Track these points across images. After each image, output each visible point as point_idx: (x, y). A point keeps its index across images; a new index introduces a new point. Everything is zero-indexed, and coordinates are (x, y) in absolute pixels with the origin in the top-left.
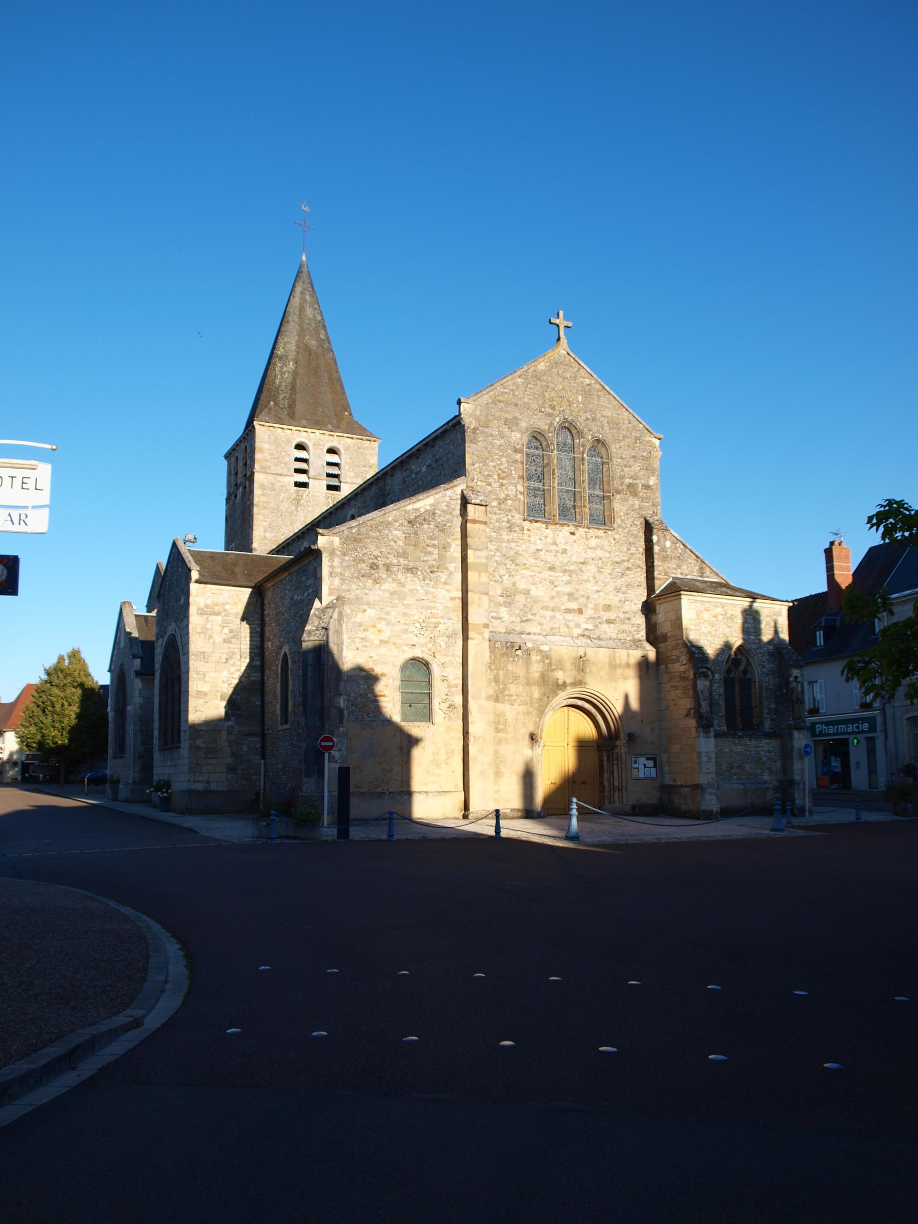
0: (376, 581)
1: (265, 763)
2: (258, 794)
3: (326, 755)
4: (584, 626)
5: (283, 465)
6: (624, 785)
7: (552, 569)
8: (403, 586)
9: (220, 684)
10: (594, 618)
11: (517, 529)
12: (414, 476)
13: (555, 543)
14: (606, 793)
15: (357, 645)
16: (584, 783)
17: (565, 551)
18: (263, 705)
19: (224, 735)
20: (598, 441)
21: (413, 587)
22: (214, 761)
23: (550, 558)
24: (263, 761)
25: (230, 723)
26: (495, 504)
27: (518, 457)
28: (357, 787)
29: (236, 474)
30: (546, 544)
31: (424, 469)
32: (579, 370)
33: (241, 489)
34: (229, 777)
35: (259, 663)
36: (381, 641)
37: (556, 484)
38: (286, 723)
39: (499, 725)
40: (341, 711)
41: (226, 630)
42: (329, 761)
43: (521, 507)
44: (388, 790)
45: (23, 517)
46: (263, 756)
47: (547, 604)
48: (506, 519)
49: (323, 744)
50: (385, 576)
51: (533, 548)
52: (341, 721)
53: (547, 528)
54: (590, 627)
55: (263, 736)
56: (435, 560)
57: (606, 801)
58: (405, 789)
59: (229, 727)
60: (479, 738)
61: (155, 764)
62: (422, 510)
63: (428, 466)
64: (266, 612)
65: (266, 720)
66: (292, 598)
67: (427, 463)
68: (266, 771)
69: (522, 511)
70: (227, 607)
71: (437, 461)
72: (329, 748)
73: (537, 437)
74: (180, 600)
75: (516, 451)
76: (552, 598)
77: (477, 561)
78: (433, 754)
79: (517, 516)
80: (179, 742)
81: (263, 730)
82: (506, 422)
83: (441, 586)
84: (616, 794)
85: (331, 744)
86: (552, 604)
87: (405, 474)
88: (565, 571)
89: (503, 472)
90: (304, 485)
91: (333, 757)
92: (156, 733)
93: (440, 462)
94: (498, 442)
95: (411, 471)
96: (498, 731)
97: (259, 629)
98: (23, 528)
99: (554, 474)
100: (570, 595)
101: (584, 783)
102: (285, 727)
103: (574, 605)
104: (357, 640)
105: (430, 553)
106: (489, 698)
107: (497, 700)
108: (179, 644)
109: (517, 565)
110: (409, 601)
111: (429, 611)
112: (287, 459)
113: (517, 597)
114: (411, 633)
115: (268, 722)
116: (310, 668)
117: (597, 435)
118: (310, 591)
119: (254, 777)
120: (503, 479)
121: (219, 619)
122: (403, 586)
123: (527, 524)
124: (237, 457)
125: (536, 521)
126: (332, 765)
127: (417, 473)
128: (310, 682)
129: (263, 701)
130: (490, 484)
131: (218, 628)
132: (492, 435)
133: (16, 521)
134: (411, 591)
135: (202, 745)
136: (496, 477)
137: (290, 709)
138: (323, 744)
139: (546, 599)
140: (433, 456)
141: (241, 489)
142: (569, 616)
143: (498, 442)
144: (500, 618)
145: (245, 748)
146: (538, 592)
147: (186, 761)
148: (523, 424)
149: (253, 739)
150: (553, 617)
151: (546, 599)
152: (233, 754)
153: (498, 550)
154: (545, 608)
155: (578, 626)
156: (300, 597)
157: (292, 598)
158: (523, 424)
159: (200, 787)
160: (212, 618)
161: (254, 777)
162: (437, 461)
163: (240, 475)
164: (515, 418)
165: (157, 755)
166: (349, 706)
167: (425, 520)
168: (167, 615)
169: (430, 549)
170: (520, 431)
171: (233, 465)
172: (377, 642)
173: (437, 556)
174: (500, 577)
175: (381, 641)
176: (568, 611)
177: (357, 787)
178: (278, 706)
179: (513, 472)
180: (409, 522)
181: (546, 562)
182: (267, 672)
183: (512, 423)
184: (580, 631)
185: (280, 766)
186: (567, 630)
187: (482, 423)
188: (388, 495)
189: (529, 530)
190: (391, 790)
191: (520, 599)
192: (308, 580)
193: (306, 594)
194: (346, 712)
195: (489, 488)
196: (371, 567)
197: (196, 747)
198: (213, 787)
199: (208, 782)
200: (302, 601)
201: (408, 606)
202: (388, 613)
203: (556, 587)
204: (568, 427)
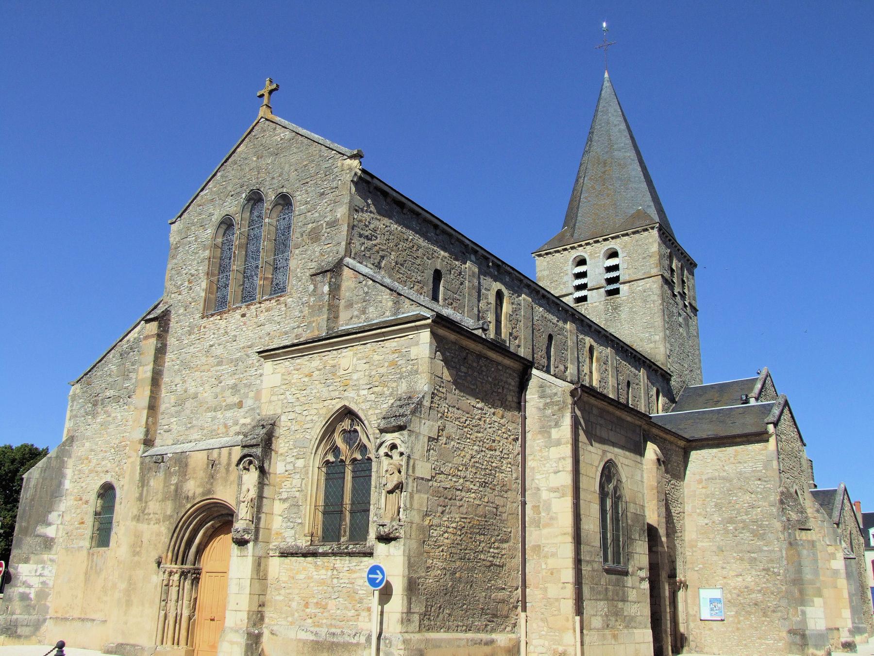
4: (242, 421)
62: (132, 339)
142: (229, 414)
146: (207, 394)
150: (213, 419)
154: (209, 409)
155: (236, 423)
172: (87, 471)
186: (224, 430)
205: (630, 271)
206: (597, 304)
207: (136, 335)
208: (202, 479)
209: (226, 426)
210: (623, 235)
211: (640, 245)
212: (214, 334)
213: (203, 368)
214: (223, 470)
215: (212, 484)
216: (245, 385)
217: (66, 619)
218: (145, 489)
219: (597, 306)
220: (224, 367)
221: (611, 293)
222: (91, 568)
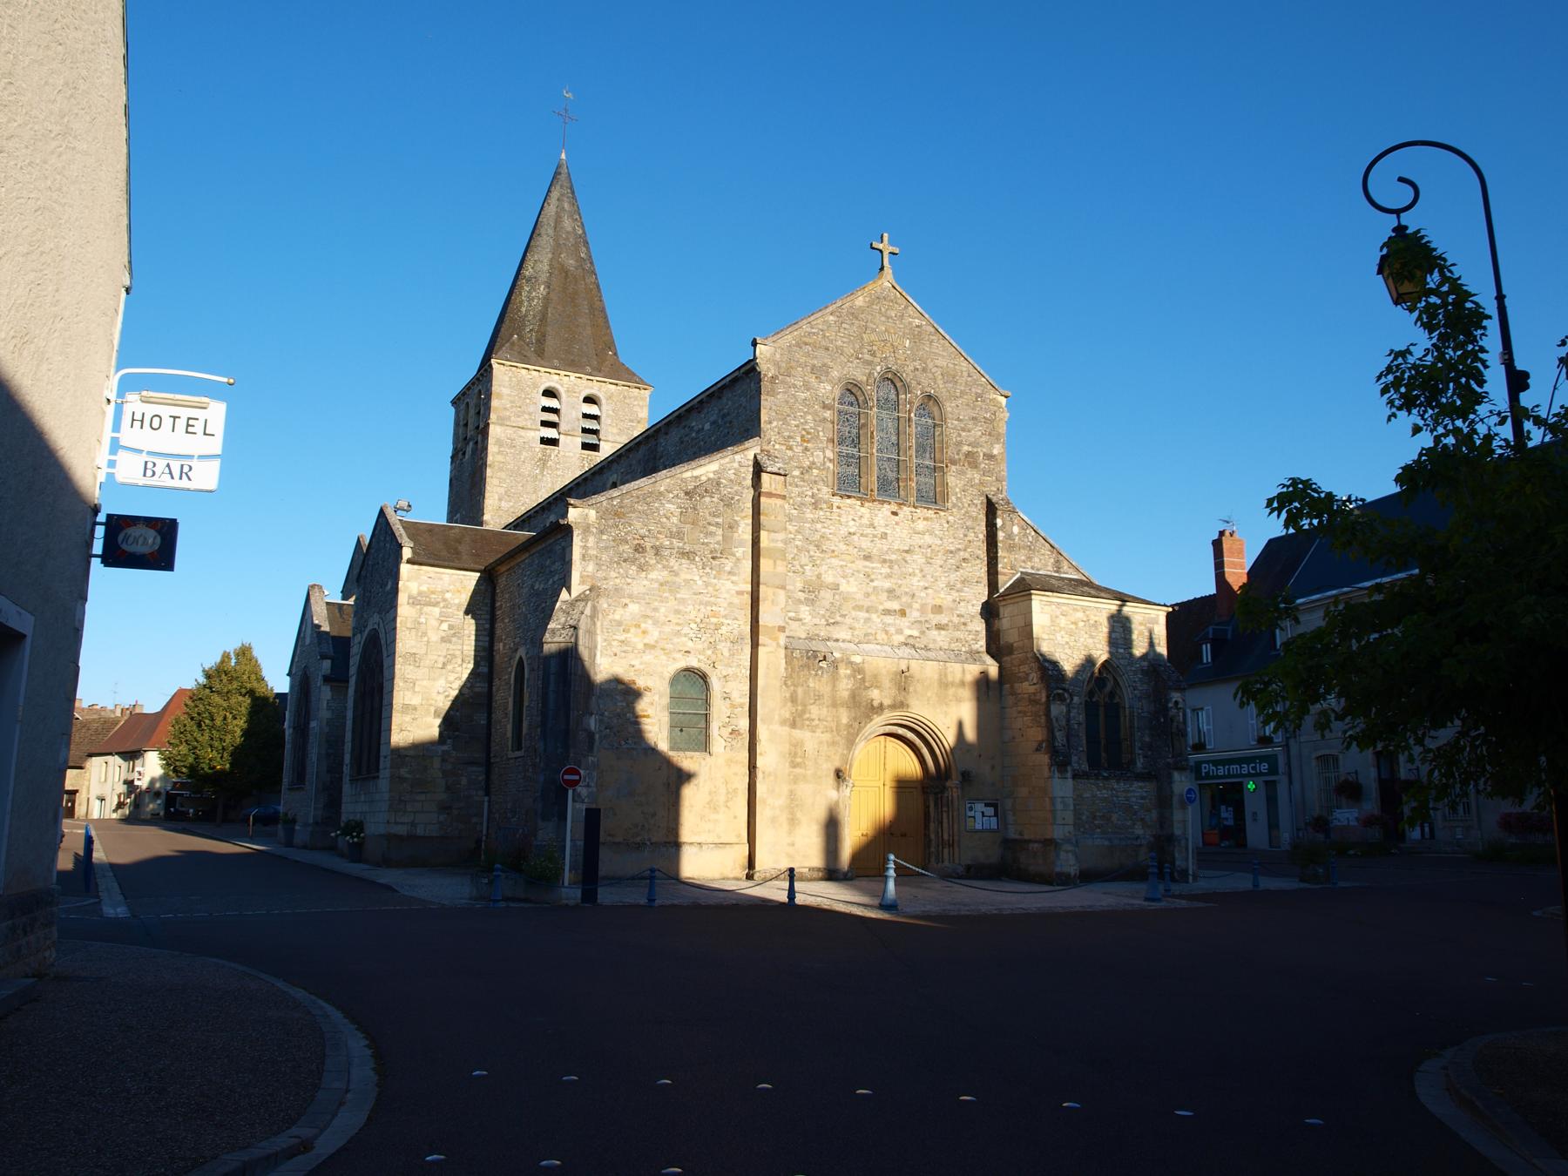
0: (641, 568)
2: (479, 841)
3: (570, 792)
4: (908, 632)
7: (867, 558)
8: (677, 574)
9: (434, 695)
13: (872, 526)
16: (903, 835)
17: (884, 536)
19: (437, 763)
25: (445, 748)
26: (796, 473)
27: (828, 414)
30: (861, 525)
31: (707, 426)
34: (442, 818)
35: (485, 670)
38: (519, 748)
39: (795, 757)
40: (591, 735)
41: (445, 626)
45: (186, 469)
46: (488, 793)
51: (844, 531)
55: (488, 766)
61: (344, 799)
63: (713, 423)
68: (490, 811)
71: (724, 416)
72: (575, 783)
73: (852, 390)
76: (867, 595)
79: (825, 489)
80: (378, 770)
86: (867, 603)
88: (885, 561)
90: (553, 442)
92: (347, 758)
95: (691, 428)
96: (794, 765)
98: (184, 483)
100: (890, 591)
101: (903, 835)
102: (518, 754)
106: (783, 722)
112: (531, 409)
115: (494, 748)
119: (474, 820)
121: (436, 610)
122: (677, 574)
123: (836, 500)
126: (578, 805)
130: (790, 448)
132: (795, 386)
133: (176, 473)
134: (687, 581)
137: (525, 731)
139: (859, 596)
142: (889, 619)
145: (464, 781)
146: (850, 587)
148: (835, 374)
151: (859, 596)
152: (448, 788)
154: (858, 608)
158: (835, 374)
159: (402, 830)
160: (427, 609)
161: (474, 820)
162: (724, 416)
163: (470, 426)
165: (347, 788)
170: (830, 382)
172: (640, 646)
176: (887, 612)
178: (510, 727)
180: (687, 493)
181: (860, 549)
182: (496, 682)
183: (820, 372)
191: (826, 595)
195: (790, 453)
198: (420, 831)
199: (413, 824)
201: (683, 601)
204: (892, 379)
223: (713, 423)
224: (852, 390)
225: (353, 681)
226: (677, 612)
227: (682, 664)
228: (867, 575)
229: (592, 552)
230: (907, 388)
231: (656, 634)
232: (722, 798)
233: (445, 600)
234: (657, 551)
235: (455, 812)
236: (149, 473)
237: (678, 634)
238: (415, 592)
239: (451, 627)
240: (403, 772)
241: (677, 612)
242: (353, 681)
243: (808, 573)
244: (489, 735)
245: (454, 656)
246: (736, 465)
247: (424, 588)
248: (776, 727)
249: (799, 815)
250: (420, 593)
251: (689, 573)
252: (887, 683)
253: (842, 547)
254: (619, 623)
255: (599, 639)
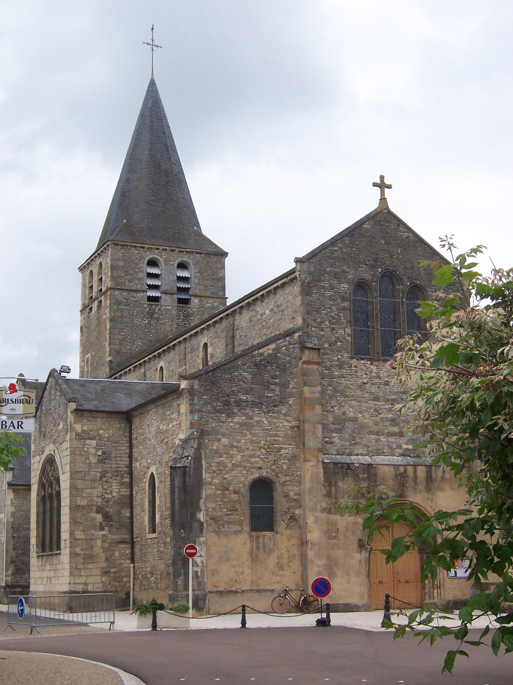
0: (228, 416)
1: (134, 567)
2: (128, 594)
3: (191, 561)
4: (405, 446)
5: (137, 282)
6: (442, 583)
7: (377, 399)
8: (251, 419)
9: (96, 499)
10: (414, 439)
11: (346, 366)
12: (259, 317)
13: (379, 377)
14: (427, 590)
15: (214, 468)
16: (407, 582)
17: (387, 383)
18: (132, 517)
19: (99, 543)
20: (416, 286)
21: (259, 419)
22: (91, 566)
23: (374, 389)
24: (132, 565)
25: (104, 533)
26: (326, 346)
27: (346, 304)
28: (215, 587)
29: (91, 287)
30: (372, 377)
31: (267, 312)
32: (398, 225)
33: (96, 302)
34: (104, 579)
35: (128, 480)
36: (233, 464)
37: (379, 326)
38: (154, 531)
39: (332, 532)
40: (201, 524)
41: (100, 453)
42: (193, 566)
43: (349, 347)
44: (240, 589)
45: (20, 423)
46: (133, 561)
47: (372, 429)
48: (336, 359)
49: (188, 551)
50: (236, 410)
51: (360, 381)
52: (202, 531)
53: (371, 364)
54: (410, 447)
55: (132, 543)
56: (277, 396)
57: (427, 597)
58: (220, 293)
59: (103, 535)
60: (315, 544)
61: (32, 569)
62: (266, 354)
63: (272, 310)
64: (134, 436)
65: (135, 529)
66: (158, 427)
67: (270, 307)
68: (135, 574)
69: (349, 350)
70: (101, 432)
71: (278, 306)
72: (193, 555)
73: (361, 286)
74: (59, 425)
75: (343, 299)
76: (377, 424)
77: (312, 396)
78: (278, 558)
79: (346, 355)
80: (59, 548)
81: (132, 538)
82: (336, 276)
83: (282, 417)
84: (435, 591)
85: (194, 551)
86: (376, 428)
87: (251, 313)
88: (388, 400)
89: (334, 318)
90: (155, 299)
91: (196, 562)
92: (33, 541)
93: (281, 308)
94: (329, 293)
95: (257, 312)
96: (330, 538)
97: (128, 451)
98: (20, 430)
99: (377, 317)
100: (392, 420)
101: (407, 582)
102: (154, 535)
103: (396, 429)
104: (214, 464)
105: (273, 390)
106: (324, 510)
107: (329, 512)
108: (58, 463)
109: (346, 396)
110: (257, 430)
111: (273, 438)
112: (140, 275)
113: (346, 423)
114: (258, 457)
115: (136, 532)
116: (176, 489)
117: (415, 281)
118: (174, 423)
119: (125, 579)
120: (334, 324)
121: (94, 443)
122: (251, 419)
123: (354, 362)
124: (91, 271)
125: (362, 359)
126: (196, 569)
127: (262, 315)
128: (177, 501)
129: (132, 512)
130: (322, 330)
131: (93, 451)
132: (324, 288)
133: (16, 426)
134: (258, 422)
135: (80, 552)
136: (327, 323)
137: (158, 520)
138: (188, 551)
139: (371, 424)
140: (276, 302)
141: (96, 304)
142: (392, 439)
143: (329, 293)
144: (332, 443)
145: (117, 554)
146: (366, 419)
147: (67, 566)
148: (350, 277)
149: (123, 546)
150: (377, 441)
151: (371, 424)
152: (107, 559)
153: (329, 385)
154: (371, 433)
155: (399, 447)
156: (165, 428)
157: (158, 427)
158: (350, 277)
159: (79, 588)
160: (88, 442)
161: (125, 579)
162: (278, 306)
163: (95, 289)
164: (344, 271)
165: (34, 560)
166: (208, 519)
167: (268, 363)
168: (44, 436)
169: (272, 387)
170: (347, 282)
171: (87, 278)
172: (230, 465)
173: (278, 393)
174: (332, 407)
175: (233, 464)
176: (391, 434)
177: (215, 587)
178: (146, 519)
179: (342, 318)
180: (255, 365)
181: (371, 393)
182: (135, 488)
183: (339, 277)
184: (401, 451)
185: (148, 570)
186: (389, 451)
187: (315, 278)
188: (237, 329)
189: (356, 367)
190: (243, 589)
191: (349, 425)
192: (173, 413)
193: (171, 425)
194: (205, 525)
195: (323, 333)
196: (225, 405)
197: (76, 554)
198: (90, 588)
199: (86, 584)
200: (167, 431)
201: (256, 435)
202: (239, 442)
203: (380, 414)
204: (389, 276)
205: (201, 287)
206: (170, 308)
207: (271, 351)
208: (393, 486)
209: (391, 447)
210: (197, 253)
211: (211, 267)
212: (366, 374)
213: (360, 399)
214: (411, 482)
215: (403, 490)
216: (404, 421)
217: (236, 592)
218: (333, 488)
219: (169, 310)
220: (381, 403)
221: (181, 301)
222: (258, 548)
223: (272, 310)
224: (361, 286)
225: (35, 488)
226: (252, 442)
227: (256, 475)
228: (376, 410)
229: (197, 407)
230: (400, 281)
231: (239, 457)
232: (286, 561)
233: (99, 435)
234: (238, 403)
235: (113, 575)
236: (4, 426)
237: (253, 456)
238: (79, 430)
239: (104, 453)
240: (78, 550)
241: (252, 442)
242: (35, 488)
243: (337, 411)
244: (132, 523)
245: (107, 472)
246: (287, 343)
247: (85, 428)
248: (318, 514)
249: (335, 570)
250: (83, 431)
251: (260, 417)
252: (391, 482)
253: (359, 393)
254: (216, 451)
255: (203, 462)
